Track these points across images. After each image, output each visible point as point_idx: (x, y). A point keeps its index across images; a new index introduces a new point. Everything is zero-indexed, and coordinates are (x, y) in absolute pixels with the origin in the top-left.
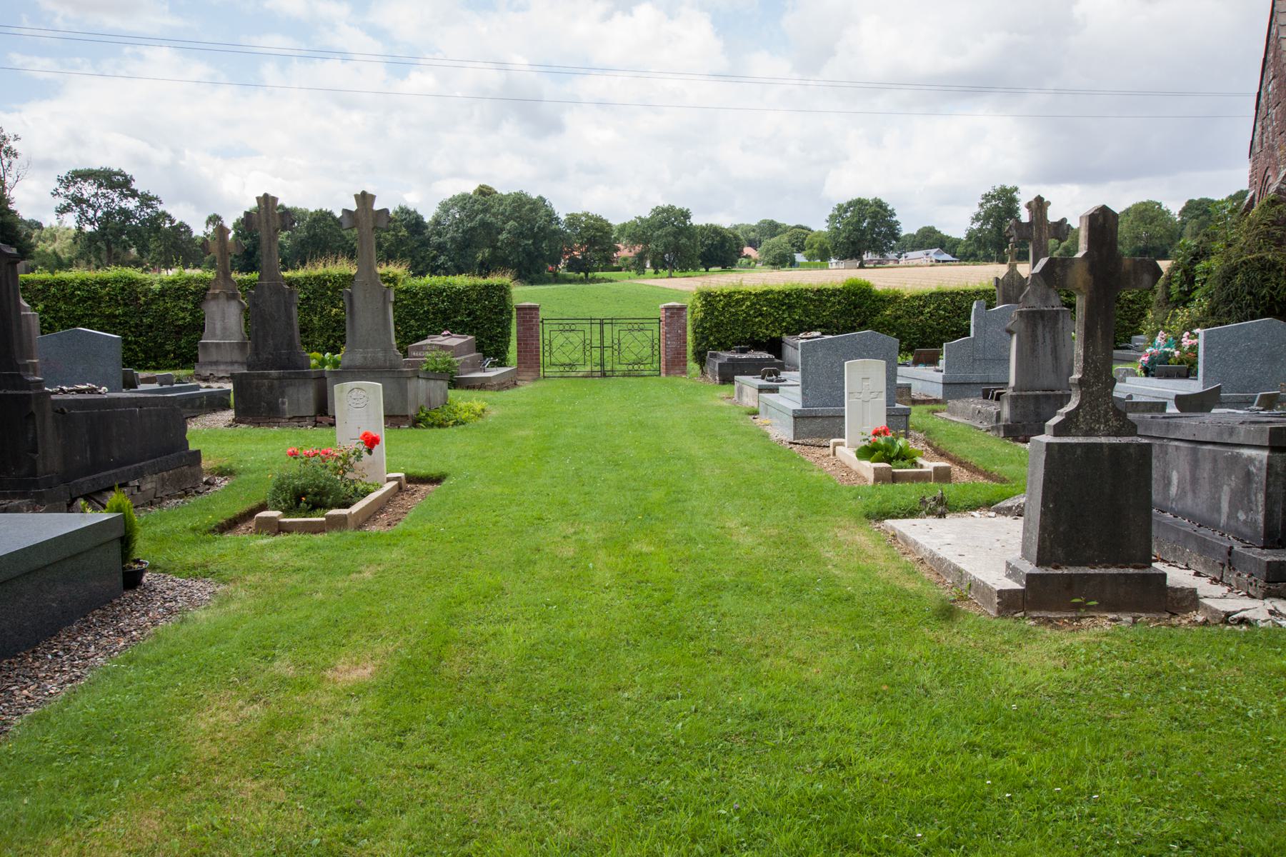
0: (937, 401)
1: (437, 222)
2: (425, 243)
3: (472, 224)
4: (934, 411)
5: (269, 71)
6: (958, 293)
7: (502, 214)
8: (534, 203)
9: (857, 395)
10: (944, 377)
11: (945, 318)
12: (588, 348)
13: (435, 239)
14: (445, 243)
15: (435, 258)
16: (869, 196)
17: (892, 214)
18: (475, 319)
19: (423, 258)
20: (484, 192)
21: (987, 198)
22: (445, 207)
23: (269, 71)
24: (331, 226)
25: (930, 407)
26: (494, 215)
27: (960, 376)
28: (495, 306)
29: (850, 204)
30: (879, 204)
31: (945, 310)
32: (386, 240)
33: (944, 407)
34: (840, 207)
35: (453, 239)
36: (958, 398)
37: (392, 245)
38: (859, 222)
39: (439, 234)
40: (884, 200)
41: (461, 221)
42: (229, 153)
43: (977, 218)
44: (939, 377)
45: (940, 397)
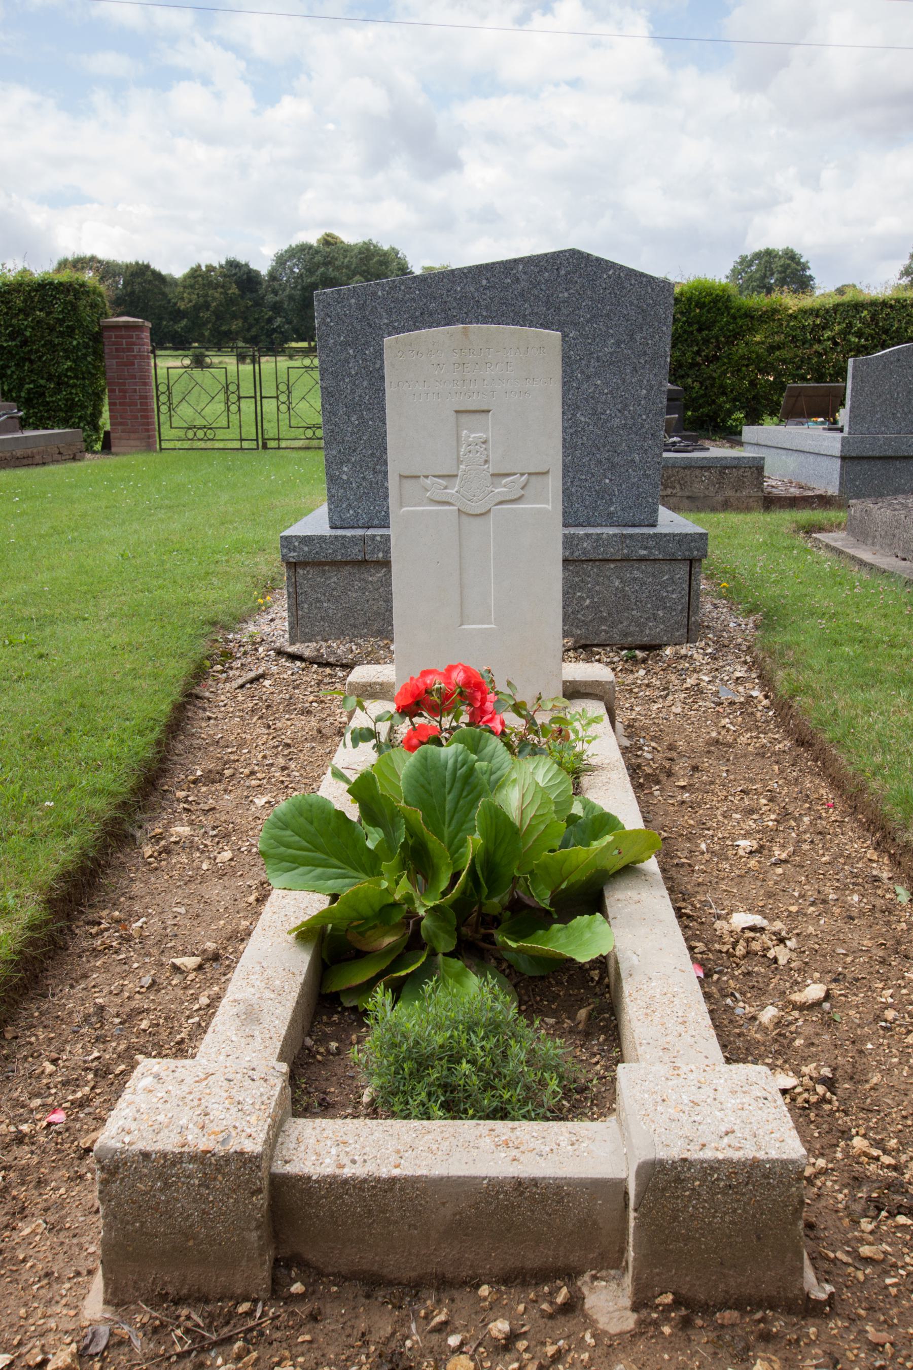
0: (824, 501)
1: (273, 276)
2: (259, 303)
3: (313, 279)
4: (809, 529)
5: (100, 97)
6: (884, 304)
7: (348, 267)
8: (385, 254)
9: (436, 488)
12: (233, 398)
13: (270, 298)
14: (281, 302)
15: (270, 320)
16: (778, 244)
17: (805, 267)
18: (25, 343)
19: (257, 320)
20: (328, 241)
22: (281, 260)
23: (100, 97)
24: (150, 282)
25: (804, 516)
26: (338, 268)
27: (886, 439)
28: (60, 321)
29: (758, 256)
30: (791, 256)
31: (859, 334)
32: (214, 299)
33: (834, 515)
34: (743, 259)
35: (291, 298)
36: (878, 494)
37: (221, 304)
38: (764, 277)
39: (275, 293)
40: (797, 251)
41: (301, 276)
42: (59, 200)
44: (832, 443)
45: (833, 490)
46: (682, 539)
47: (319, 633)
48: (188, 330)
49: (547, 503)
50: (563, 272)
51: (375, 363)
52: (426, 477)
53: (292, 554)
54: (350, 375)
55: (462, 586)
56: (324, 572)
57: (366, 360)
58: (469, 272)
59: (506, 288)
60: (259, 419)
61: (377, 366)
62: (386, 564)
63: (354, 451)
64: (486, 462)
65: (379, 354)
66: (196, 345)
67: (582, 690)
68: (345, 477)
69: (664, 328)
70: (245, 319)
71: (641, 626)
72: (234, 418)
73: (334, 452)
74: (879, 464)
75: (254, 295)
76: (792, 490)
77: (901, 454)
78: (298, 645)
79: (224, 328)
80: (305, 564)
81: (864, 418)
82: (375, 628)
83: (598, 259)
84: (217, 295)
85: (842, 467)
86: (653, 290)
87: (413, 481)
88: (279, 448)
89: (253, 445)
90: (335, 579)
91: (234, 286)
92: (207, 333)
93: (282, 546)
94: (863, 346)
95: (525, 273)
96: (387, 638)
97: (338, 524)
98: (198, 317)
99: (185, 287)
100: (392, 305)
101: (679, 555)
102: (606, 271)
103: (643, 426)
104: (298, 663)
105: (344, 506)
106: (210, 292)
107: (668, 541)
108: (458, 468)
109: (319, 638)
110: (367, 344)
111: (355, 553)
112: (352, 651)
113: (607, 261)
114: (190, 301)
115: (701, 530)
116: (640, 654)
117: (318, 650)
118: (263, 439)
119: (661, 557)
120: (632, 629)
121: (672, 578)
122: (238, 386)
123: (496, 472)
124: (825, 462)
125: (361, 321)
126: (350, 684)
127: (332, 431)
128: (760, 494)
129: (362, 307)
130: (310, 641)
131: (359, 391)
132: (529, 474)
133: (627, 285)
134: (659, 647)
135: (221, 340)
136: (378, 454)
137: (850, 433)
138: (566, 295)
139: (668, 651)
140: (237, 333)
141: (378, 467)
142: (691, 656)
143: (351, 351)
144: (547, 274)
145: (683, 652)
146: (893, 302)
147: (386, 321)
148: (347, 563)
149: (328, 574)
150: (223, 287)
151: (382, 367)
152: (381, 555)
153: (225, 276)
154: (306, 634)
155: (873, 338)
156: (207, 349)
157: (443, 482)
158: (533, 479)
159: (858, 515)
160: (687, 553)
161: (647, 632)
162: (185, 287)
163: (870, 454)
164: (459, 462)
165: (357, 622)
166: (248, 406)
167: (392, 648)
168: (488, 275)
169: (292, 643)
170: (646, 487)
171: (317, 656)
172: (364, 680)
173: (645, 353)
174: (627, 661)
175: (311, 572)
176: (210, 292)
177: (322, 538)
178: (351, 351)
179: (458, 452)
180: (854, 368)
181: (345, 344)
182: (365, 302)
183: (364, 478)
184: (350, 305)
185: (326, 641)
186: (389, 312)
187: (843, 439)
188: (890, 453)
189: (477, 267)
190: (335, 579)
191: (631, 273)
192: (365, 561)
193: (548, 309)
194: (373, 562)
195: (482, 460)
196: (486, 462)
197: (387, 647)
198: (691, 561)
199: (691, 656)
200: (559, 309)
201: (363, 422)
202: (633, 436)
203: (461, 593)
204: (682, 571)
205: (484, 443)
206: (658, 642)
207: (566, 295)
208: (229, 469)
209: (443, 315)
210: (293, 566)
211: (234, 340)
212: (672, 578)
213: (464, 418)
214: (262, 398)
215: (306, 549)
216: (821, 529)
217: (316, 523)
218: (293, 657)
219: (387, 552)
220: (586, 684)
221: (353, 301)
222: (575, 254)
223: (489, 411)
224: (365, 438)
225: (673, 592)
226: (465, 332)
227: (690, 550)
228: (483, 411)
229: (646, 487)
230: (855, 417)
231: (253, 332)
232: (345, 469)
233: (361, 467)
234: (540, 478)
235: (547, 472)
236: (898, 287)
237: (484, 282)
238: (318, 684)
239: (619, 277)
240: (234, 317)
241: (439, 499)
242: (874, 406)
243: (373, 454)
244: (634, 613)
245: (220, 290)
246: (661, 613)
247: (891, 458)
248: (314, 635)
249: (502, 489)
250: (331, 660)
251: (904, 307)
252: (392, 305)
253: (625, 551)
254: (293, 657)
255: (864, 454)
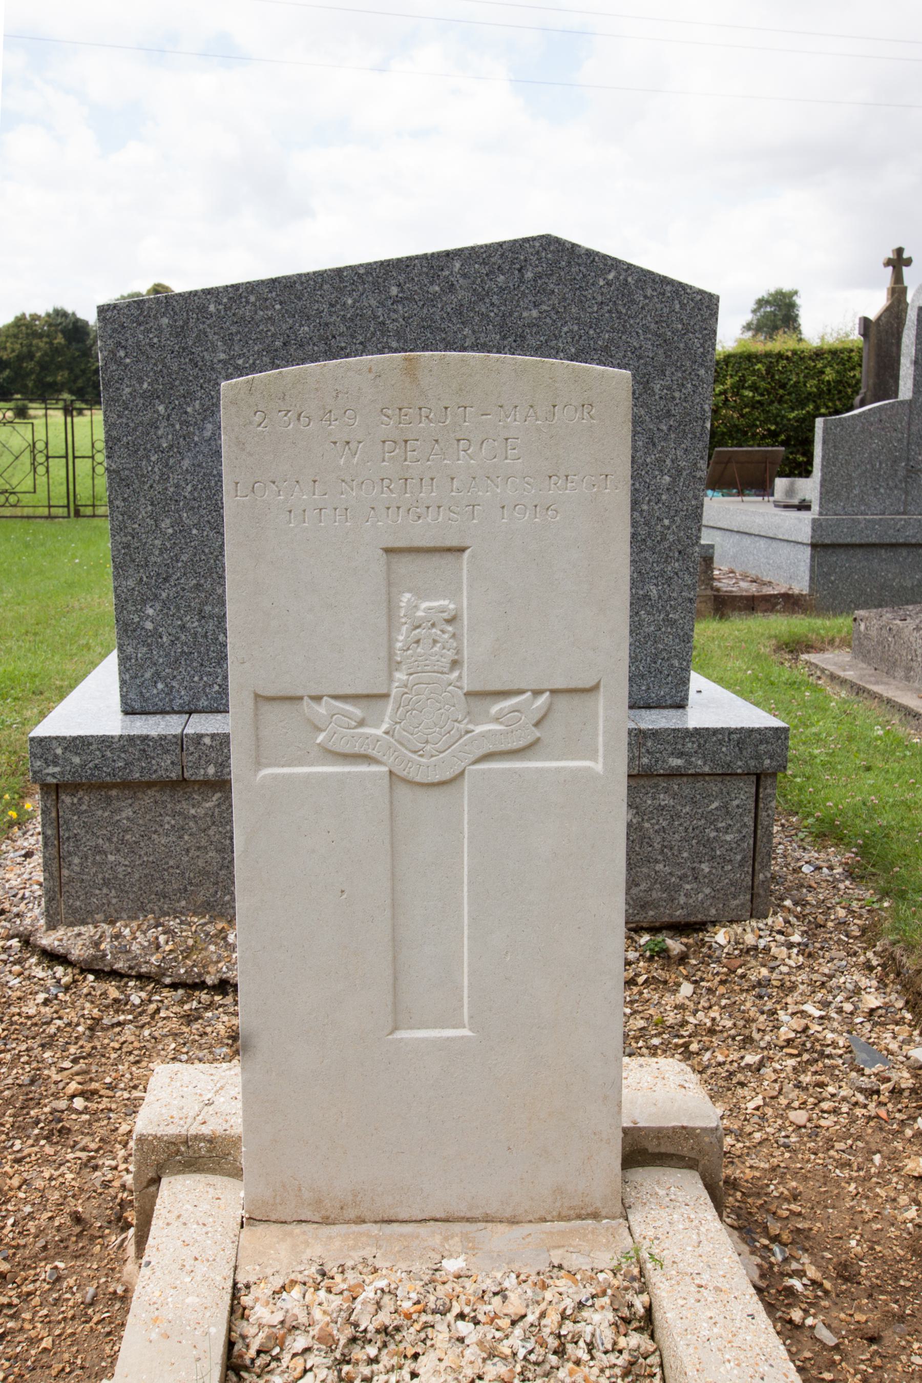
0: (790, 603)
4: (795, 647)
9: (336, 722)
10: (816, 525)
11: (754, 405)
12: (41, 458)
19: (83, 371)
20: (157, 289)
21: (761, 303)
27: (872, 519)
31: (754, 388)
32: (39, 349)
37: (46, 354)
43: (748, 327)
44: (800, 526)
45: (801, 586)
46: (743, 738)
47: (98, 909)
48: (10, 380)
49: (596, 760)
50: (529, 275)
51: (202, 429)
52: (317, 698)
53: (52, 770)
54: (158, 449)
55: (395, 942)
56: (109, 800)
57: (187, 423)
58: (368, 273)
59: (431, 301)
60: (71, 480)
61: (207, 434)
62: (221, 785)
63: (166, 580)
64: (455, 664)
65: (211, 409)
66: (19, 396)
67: (652, 1147)
68: (149, 625)
69: (702, 372)
70: (71, 370)
71: (672, 890)
72: (42, 480)
73: (131, 583)
74: (860, 553)
75: (80, 345)
76: (743, 585)
77: (887, 540)
78: (61, 932)
79: (49, 379)
80: (74, 787)
81: (838, 495)
82: (200, 899)
83: (590, 253)
84: (42, 345)
85: (813, 557)
86: (683, 306)
87: (286, 707)
88: (94, 516)
89: (62, 511)
90: (128, 812)
91: (60, 335)
92: (30, 384)
93: (33, 755)
94: (759, 402)
95: (465, 276)
96: (222, 915)
97: (137, 706)
98: (21, 367)
99: (7, 336)
100: (234, 329)
101: (739, 766)
102: (603, 273)
103: (664, 538)
104: (59, 970)
105: (148, 675)
106: (35, 342)
107: (720, 742)
108: (391, 679)
109: (99, 917)
110: (189, 396)
111: (165, 766)
112: (158, 947)
113: (605, 257)
114: (13, 351)
115: (781, 724)
116: (675, 945)
117: (97, 944)
118: (76, 506)
119: (707, 769)
120: (655, 895)
121: (725, 806)
122: (47, 444)
123: (478, 687)
124: (786, 549)
125: (179, 356)
126: (141, 1140)
127: (127, 546)
128: (709, 592)
129: (180, 332)
130: (84, 923)
131: (174, 478)
132: (553, 692)
133: (639, 297)
134: (700, 927)
135: (45, 393)
136: (208, 586)
137: (821, 514)
138: (535, 313)
139: (721, 936)
140: (63, 384)
141: (208, 608)
142: (767, 949)
143: (161, 408)
144: (501, 278)
145: (750, 939)
146: (789, 354)
147: (223, 356)
148: (150, 785)
149: (116, 804)
150: (48, 336)
151: (216, 436)
152: (211, 770)
153: (50, 325)
154: (75, 911)
155: (769, 394)
156: (31, 401)
157: (355, 710)
158: (562, 702)
159: (873, 633)
160: (752, 763)
161: (682, 900)
162: (7, 336)
163: (848, 540)
164: (393, 665)
165: (169, 889)
166: (58, 468)
167: (231, 938)
168: (401, 278)
169: (52, 926)
170: (669, 640)
171: (95, 958)
172: (172, 1130)
173: (669, 414)
174: (651, 959)
175: (86, 800)
176: (35, 342)
177: (105, 741)
178: (161, 408)
179: (391, 641)
180: (826, 430)
181: (152, 396)
182: (186, 323)
183: (183, 627)
184: (160, 329)
185: (112, 923)
186: (229, 340)
187: (814, 521)
188: (873, 539)
189: (382, 263)
190: (128, 812)
191: (647, 278)
192: (183, 781)
193: (504, 338)
194: (194, 782)
195: (446, 662)
196: (455, 664)
197: (222, 935)
198: (758, 776)
199: (767, 949)
200: (523, 338)
201: (181, 529)
202: (647, 554)
203: (395, 958)
204: (741, 795)
205: (449, 621)
206: (700, 917)
207: (535, 313)
208: (27, 546)
209: (322, 347)
210: (53, 791)
211: (60, 391)
212: (725, 806)
213: (405, 566)
214: (66, 457)
215: (77, 760)
216: (809, 648)
217: (93, 707)
218: (52, 957)
219: (224, 764)
220: (659, 1133)
221: (165, 321)
222: (549, 243)
223: (462, 550)
224: (184, 558)
225: (727, 829)
226: (410, 371)
227: (758, 757)
228: (449, 550)
229: (669, 640)
230: (827, 492)
231: (80, 383)
232: (150, 611)
233: (178, 608)
234: (576, 700)
235: (595, 688)
236: (739, 341)
237: (394, 291)
238: (91, 1029)
239: (626, 283)
240: (60, 367)
241: (347, 750)
242: (850, 478)
243: (198, 586)
244: (660, 867)
245: (45, 339)
246: (706, 868)
247: (874, 545)
248: (90, 913)
249: (487, 728)
250: (119, 966)
251: (801, 359)
252: (234, 329)
253: (645, 761)
254: (52, 957)
255: (841, 541)
